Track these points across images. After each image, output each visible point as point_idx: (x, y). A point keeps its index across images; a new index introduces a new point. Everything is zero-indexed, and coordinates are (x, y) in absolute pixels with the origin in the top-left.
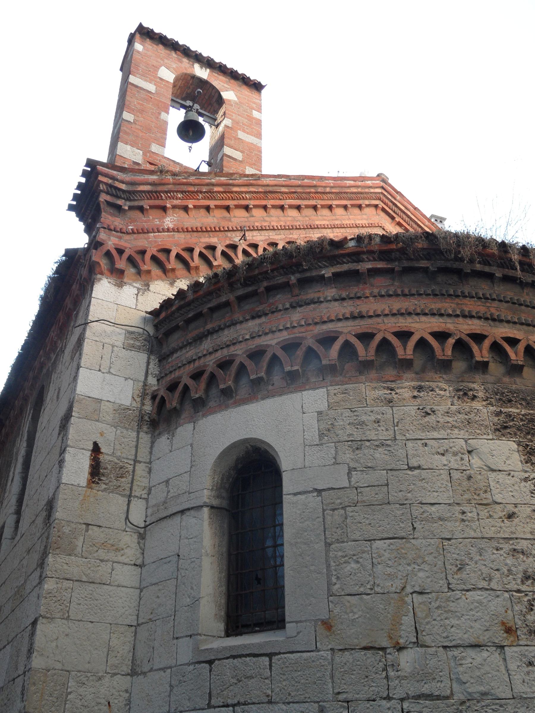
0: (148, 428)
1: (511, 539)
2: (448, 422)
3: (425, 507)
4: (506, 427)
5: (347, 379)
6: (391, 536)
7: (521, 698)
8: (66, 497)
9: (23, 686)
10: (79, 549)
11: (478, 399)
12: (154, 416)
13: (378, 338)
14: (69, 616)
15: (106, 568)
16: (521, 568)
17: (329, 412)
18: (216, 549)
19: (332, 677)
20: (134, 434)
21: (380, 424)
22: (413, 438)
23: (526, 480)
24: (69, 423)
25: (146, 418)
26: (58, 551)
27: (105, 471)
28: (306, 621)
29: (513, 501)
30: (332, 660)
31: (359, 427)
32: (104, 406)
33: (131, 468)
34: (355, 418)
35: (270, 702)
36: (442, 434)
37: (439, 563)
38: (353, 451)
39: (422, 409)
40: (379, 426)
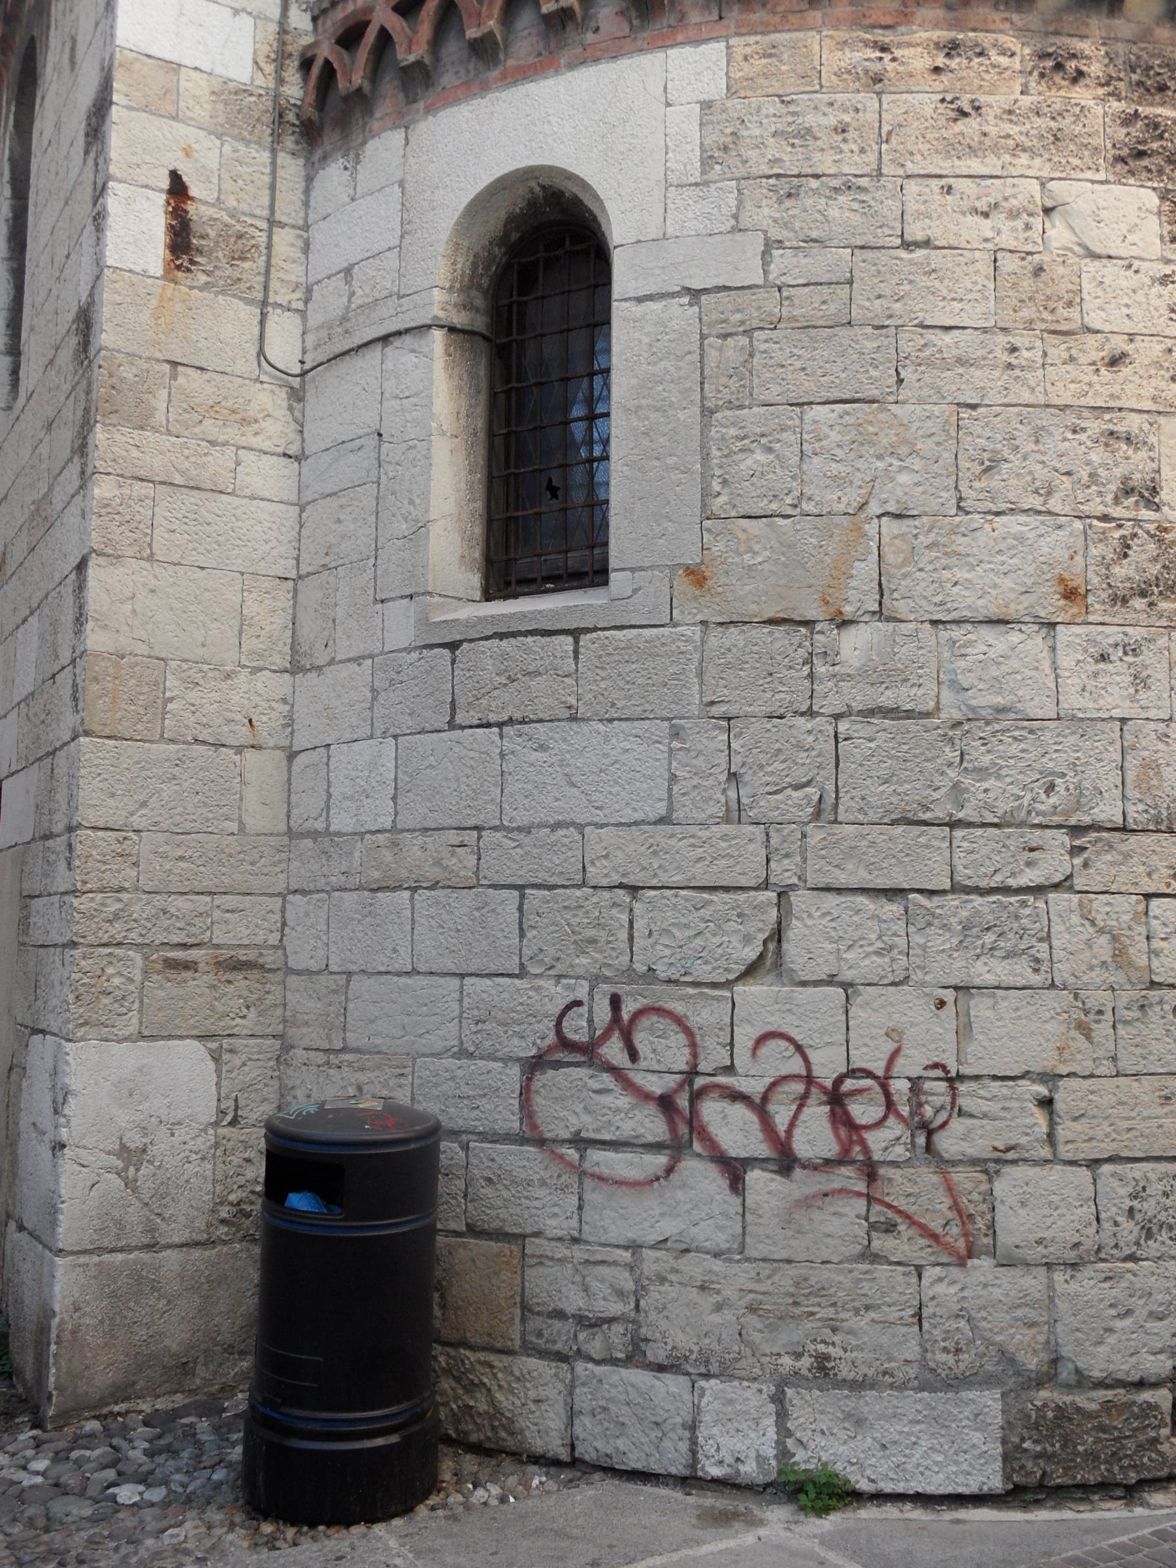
0: (297, 143)
1: (1109, 409)
2: (1008, 136)
3: (930, 335)
4: (1141, 154)
5: (777, 19)
6: (847, 396)
7: (1073, 718)
8: (118, 299)
9: (75, 685)
10: (160, 417)
11: (1088, 81)
14: (152, 554)
15: (220, 460)
16: (1118, 472)
17: (729, 104)
18: (463, 422)
19: (700, 674)
20: (265, 156)
21: (849, 136)
22: (922, 172)
24: (108, 122)
25: (291, 117)
26: (114, 419)
27: (203, 242)
28: (651, 568)
29: (1129, 327)
30: (703, 642)
31: (796, 141)
32: (191, 84)
33: (262, 238)
34: (790, 119)
35: (574, 719)
36: (991, 165)
37: (945, 455)
38: (780, 201)
39: (952, 102)
40: (845, 140)
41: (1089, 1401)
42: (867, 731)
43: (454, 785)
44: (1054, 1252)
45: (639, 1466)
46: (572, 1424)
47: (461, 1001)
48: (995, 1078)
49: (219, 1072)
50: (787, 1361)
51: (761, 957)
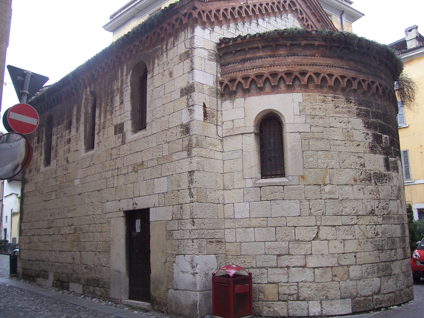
3: (335, 141)
4: (359, 114)
12: (223, 92)
13: (322, 75)
15: (212, 153)
19: (304, 193)
20: (216, 99)
23: (364, 133)
32: (206, 88)
33: (216, 113)
35: (284, 200)
41: (362, 299)
42: (329, 201)
43: (262, 210)
44: (357, 278)
45: (300, 316)
46: (288, 311)
47: (265, 246)
48: (349, 253)
49: (217, 260)
50: (321, 297)
51: (316, 237)
